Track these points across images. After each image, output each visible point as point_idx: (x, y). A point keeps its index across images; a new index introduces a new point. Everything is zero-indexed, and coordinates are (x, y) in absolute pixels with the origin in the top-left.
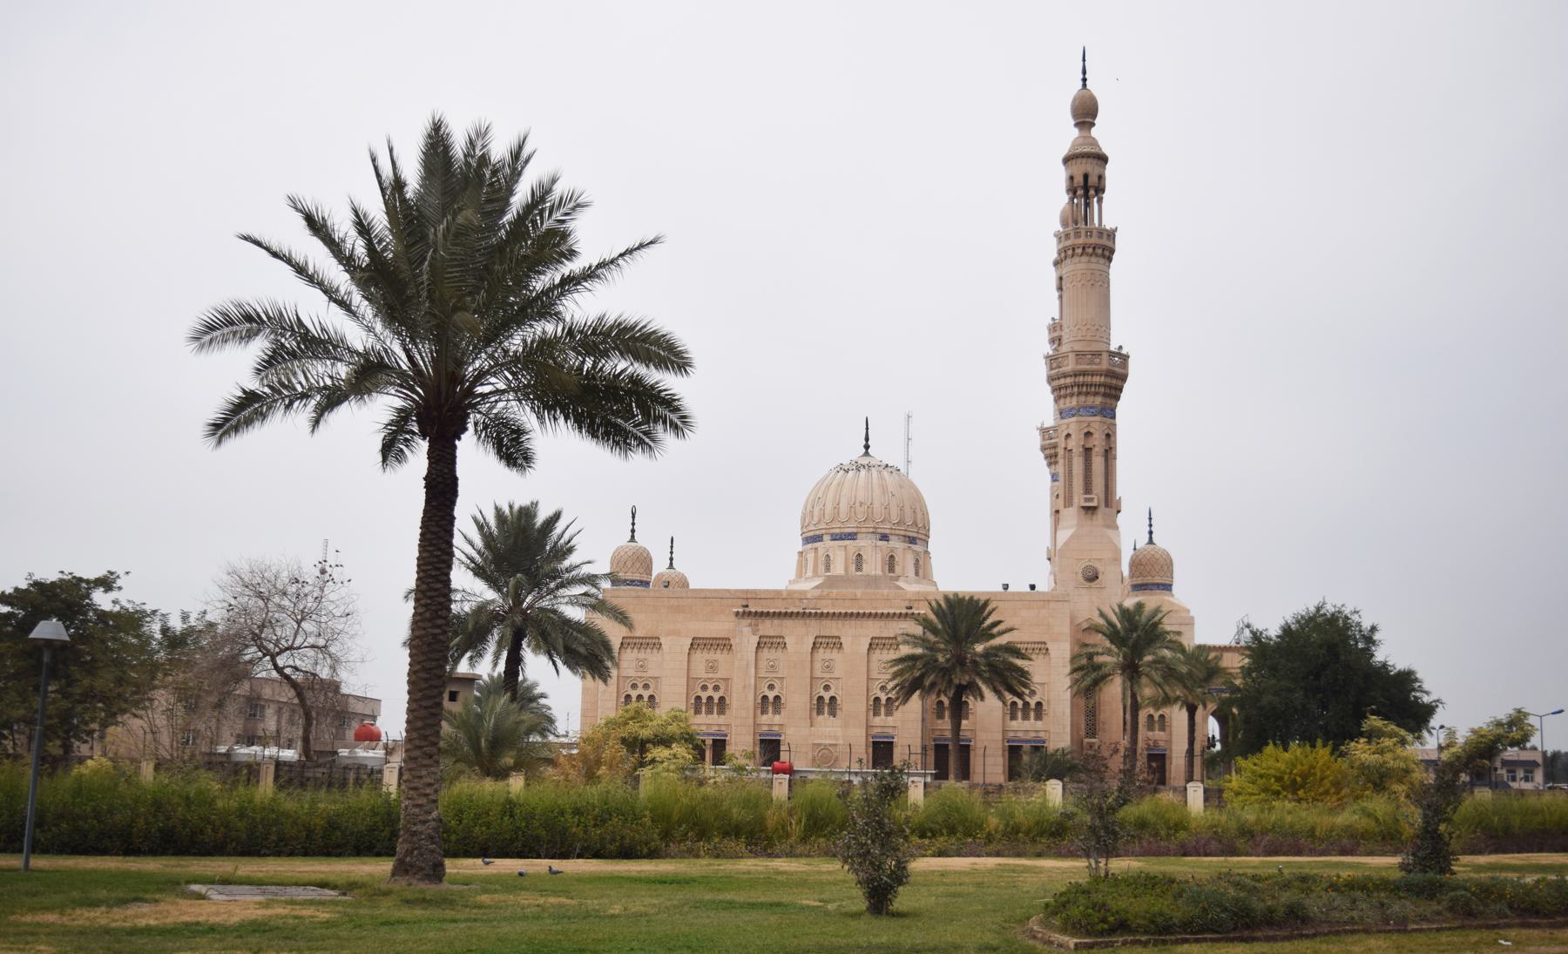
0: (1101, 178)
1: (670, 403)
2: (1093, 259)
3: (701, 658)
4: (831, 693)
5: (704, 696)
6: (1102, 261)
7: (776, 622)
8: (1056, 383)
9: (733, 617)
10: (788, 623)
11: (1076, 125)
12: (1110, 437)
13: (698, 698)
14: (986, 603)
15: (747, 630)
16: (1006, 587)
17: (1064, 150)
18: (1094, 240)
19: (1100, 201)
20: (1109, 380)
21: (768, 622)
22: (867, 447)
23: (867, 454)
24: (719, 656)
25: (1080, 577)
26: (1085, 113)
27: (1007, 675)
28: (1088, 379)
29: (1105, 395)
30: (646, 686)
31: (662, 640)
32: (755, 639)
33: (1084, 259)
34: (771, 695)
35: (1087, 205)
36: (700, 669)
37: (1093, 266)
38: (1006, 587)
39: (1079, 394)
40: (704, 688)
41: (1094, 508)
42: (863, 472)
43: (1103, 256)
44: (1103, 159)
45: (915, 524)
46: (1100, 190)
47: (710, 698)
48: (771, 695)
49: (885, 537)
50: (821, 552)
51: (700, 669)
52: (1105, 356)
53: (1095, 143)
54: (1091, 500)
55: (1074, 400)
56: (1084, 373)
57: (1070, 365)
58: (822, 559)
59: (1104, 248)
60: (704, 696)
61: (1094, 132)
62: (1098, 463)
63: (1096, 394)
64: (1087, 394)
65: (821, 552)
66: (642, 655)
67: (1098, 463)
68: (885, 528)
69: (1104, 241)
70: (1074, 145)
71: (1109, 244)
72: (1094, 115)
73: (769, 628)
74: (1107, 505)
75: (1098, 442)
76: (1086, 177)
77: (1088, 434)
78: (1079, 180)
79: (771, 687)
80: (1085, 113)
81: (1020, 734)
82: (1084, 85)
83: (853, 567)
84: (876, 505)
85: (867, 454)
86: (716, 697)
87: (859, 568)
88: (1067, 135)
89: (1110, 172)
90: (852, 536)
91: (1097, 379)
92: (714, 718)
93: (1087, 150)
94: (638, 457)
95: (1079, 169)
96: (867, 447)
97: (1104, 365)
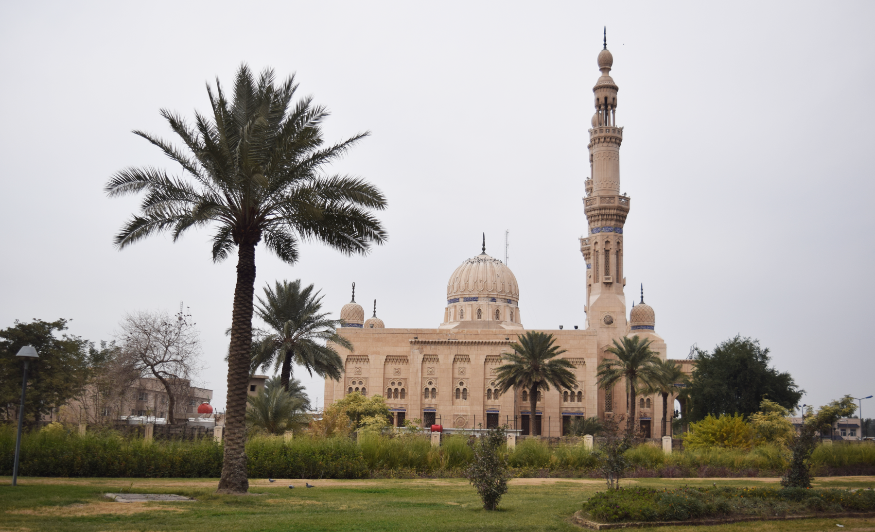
0: (614, 99)
2: (610, 144)
3: (391, 367)
4: (464, 386)
5: (393, 388)
6: (615, 145)
7: (433, 347)
8: (590, 214)
10: (440, 347)
14: (550, 337)
15: (417, 351)
16: (561, 327)
17: (594, 84)
18: (611, 134)
19: (614, 112)
21: (428, 347)
22: (484, 249)
23: (484, 253)
24: (401, 366)
26: (606, 63)
27: (562, 376)
28: (607, 211)
29: (616, 220)
30: (361, 383)
31: (370, 357)
32: (421, 357)
33: (605, 144)
35: (607, 114)
36: (390, 374)
37: (610, 148)
38: (561, 327)
41: (611, 283)
42: (482, 263)
43: (616, 143)
44: (616, 89)
45: (511, 292)
46: (614, 106)
47: (396, 389)
49: (494, 300)
51: (390, 374)
52: (617, 198)
53: (611, 80)
54: (609, 279)
55: (613, 223)
56: (605, 208)
57: (597, 204)
58: (459, 312)
59: (616, 138)
60: (393, 388)
61: (611, 74)
62: (613, 258)
63: (611, 220)
64: (607, 220)
65: (458, 308)
66: (358, 365)
67: (613, 258)
68: (494, 295)
69: (616, 135)
70: (599, 81)
71: (619, 136)
72: (611, 64)
73: (429, 350)
75: (612, 246)
76: (606, 98)
77: (607, 242)
78: (602, 100)
79: (430, 383)
80: (606, 63)
81: (569, 410)
82: (605, 48)
83: (476, 316)
84: (489, 282)
85: (484, 253)
86: (400, 388)
87: (479, 317)
88: (595, 75)
89: (620, 96)
90: (475, 299)
91: (612, 211)
92: (399, 401)
93: (607, 83)
95: (602, 94)
96: (484, 249)
97: (616, 203)
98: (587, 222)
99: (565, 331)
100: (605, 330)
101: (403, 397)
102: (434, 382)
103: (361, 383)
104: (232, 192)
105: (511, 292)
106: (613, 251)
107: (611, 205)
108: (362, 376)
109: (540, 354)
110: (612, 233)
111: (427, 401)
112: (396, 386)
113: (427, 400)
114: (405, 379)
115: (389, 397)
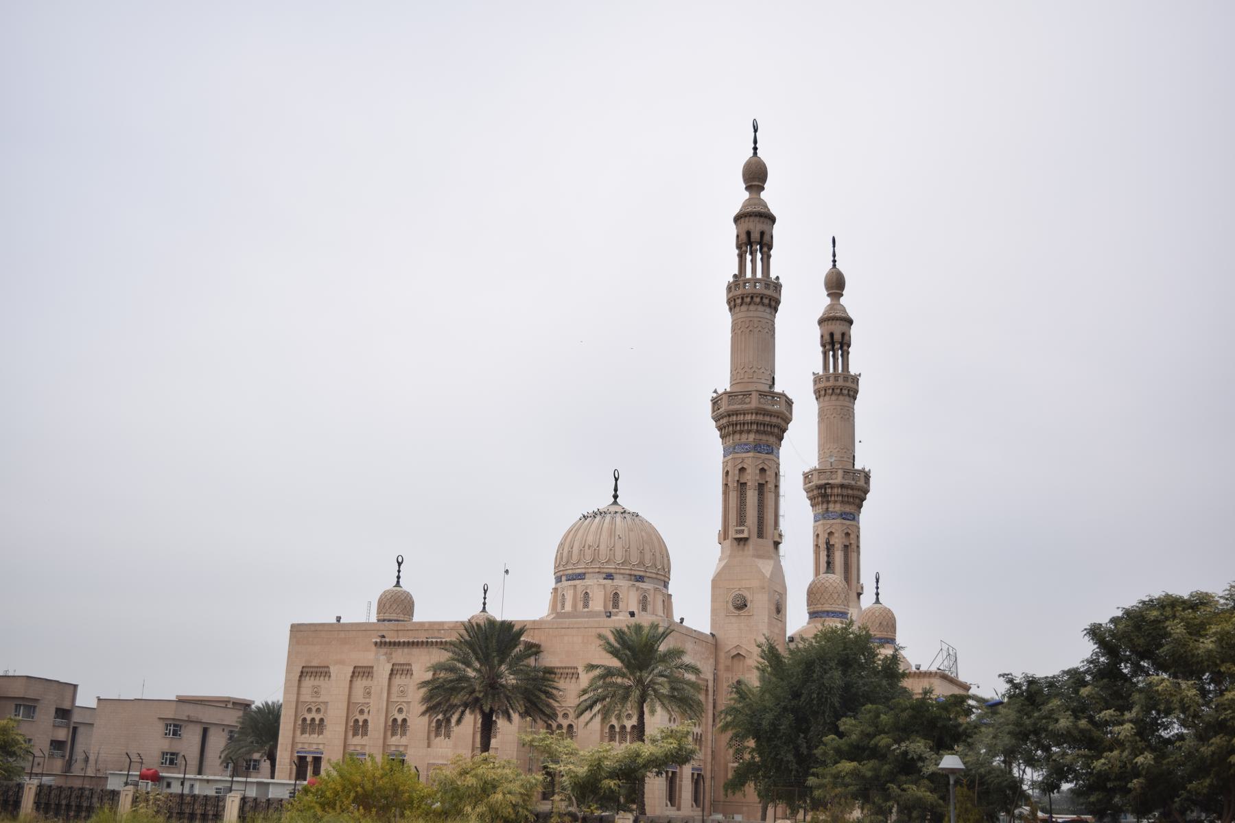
2: (752, 307)
4: (365, 716)
5: (309, 717)
6: (768, 310)
7: (406, 650)
8: (724, 421)
9: (374, 648)
10: (415, 651)
11: (747, 188)
13: (395, 720)
14: (521, 632)
15: (383, 658)
16: (339, 619)
17: (736, 210)
20: (760, 418)
21: (400, 651)
22: (616, 497)
23: (615, 503)
25: (732, 608)
26: (755, 176)
27: (536, 697)
28: (741, 418)
29: (757, 432)
30: (318, 710)
31: (332, 669)
32: (389, 667)
33: (744, 308)
34: (400, 718)
37: (751, 314)
38: (339, 619)
39: (734, 432)
40: (309, 710)
41: (746, 539)
42: (608, 517)
43: (770, 306)
45: (642, 563)
47: (313, 719)
48: (400, 718)
49: (609, 576)
50: (579, 589)
51: (307, 696)
54: (742, 531)
55: (752, 437)
56: (736, 413)
57: (724, 407)
58: (580, 595)
59: (771, 299)
60: (309, 717)
61: (763, 195)
62: (752, 496)
63: (749, 432)
64: (741, 432)
65: (579, 589)
66: (317, 683)
68: (610, 568)
70: (744, 206)
71: (774, 295)
73: (400, 656)
74: (761, 535)
77: (742, 470)
79: (400, 711)
80: (755, 176)
81: (359, 748)
82: (755, 153)
83: (580, 605)
84: (602, 547)
85: (615, 503)
87: (586, 605)
88: (739, 196)
90: (581, 576)
91: (748, 418)
93: (758, 209)
96: (616, 497)
98: (718, 433)
99: (687, 628)
100: (733, 620)
103: (318, 710)
105: (642, 563)
107: (745, 406)
108: (320, 700)
109: (953, 681)
110: (751, 454)
111: (394, 740)
112: (314, 715)
113: (394, 738)
114: (326, 703)
115: (303, 732)
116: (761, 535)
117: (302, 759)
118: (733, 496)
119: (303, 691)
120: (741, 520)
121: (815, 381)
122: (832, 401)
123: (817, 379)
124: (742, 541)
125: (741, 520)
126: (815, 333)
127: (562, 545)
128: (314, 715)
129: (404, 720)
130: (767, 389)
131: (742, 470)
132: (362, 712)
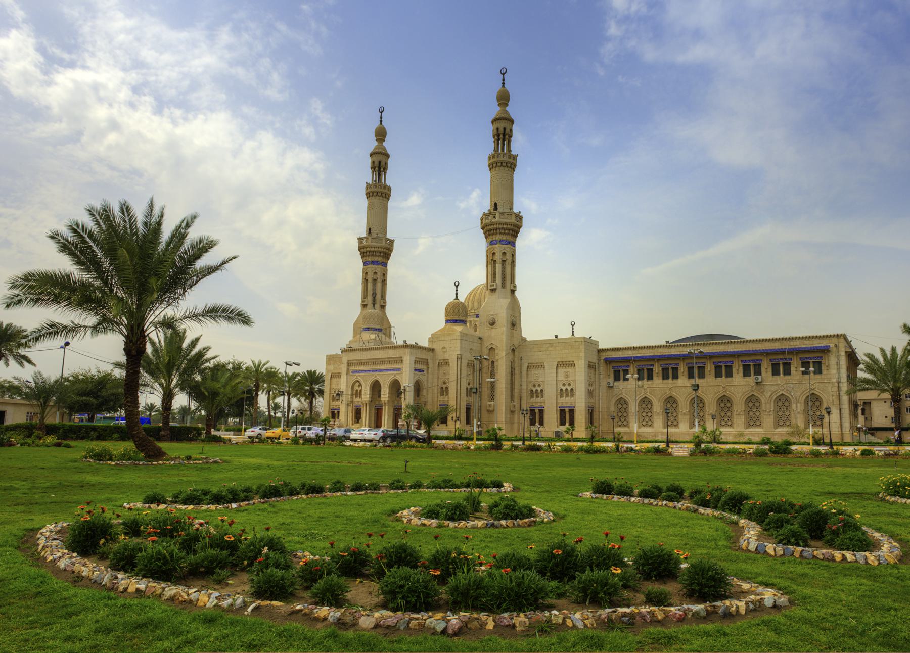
0: (386, 164)
1: (65, 247)
3: (562, 371)
5: (564, 388)
12: (384, 275)
16: (556, 336)
17: (371, 150)
18: (382, 190)
19: (385, 174)
24: (570, 370)
30: (569, 384)
31: (546, 365)
34: (444, 386)
35: (380, 175)
36: (561, 377)
38: (556, 336)
44: (388, 156)
46: (385, 169)
52: (384, 240)
53: (385, 149)
60: (564, 388)
61: (507, 108)
62: (379, 285)
67: (379, 285)
69: (386, 191)
70: (376, 148)
72: (385, 137)
74: (503, 286)
75: (379, 276)
76: (380, 162)
78: (377, 164)
86: (539, 389)
88: (373, 144)
89: (391, 162)
92: (568, 399)
94: (20, 271)
95: (377, 158)
97: (384, 244)
101: (572, 395)
102: (572, 383)
103: (569, 384)
104: (125, 227)
106: (379, 280)
116: (503, 286)
117: (532, 412)
118: (490, 266)
119: (559, 375)
120: (494, 280)
121: (367, 188)
122: (376, 200)
123: (368, 186)
124: (493, 290)
125: (494, 280)
126: (368, 161)
127: (470, 294)
128: (537, 388)
129: (572, 389)
130: (507, 211)
131: (494, 254)
132: (534, 386)
